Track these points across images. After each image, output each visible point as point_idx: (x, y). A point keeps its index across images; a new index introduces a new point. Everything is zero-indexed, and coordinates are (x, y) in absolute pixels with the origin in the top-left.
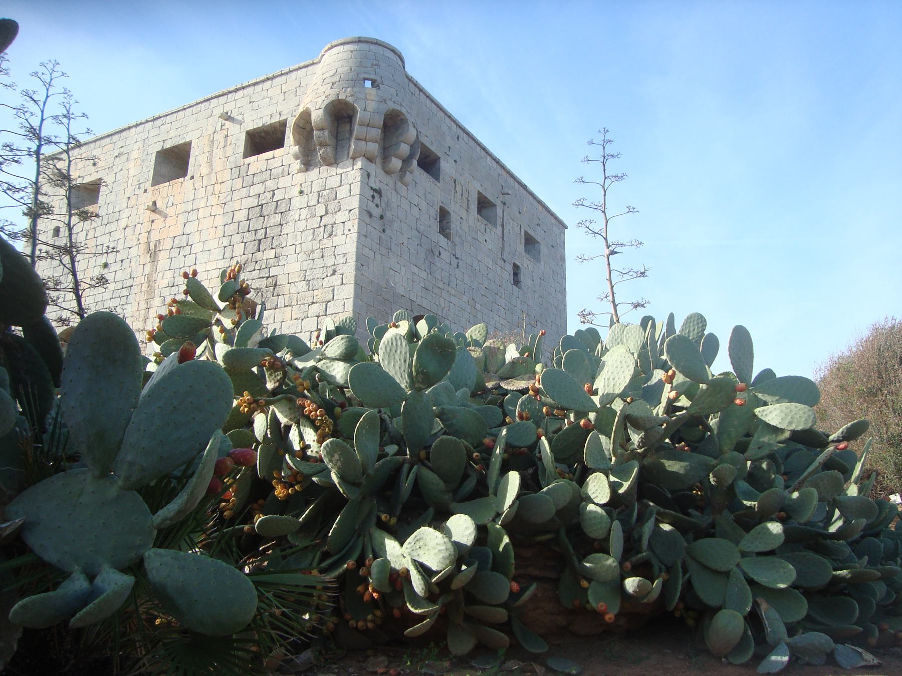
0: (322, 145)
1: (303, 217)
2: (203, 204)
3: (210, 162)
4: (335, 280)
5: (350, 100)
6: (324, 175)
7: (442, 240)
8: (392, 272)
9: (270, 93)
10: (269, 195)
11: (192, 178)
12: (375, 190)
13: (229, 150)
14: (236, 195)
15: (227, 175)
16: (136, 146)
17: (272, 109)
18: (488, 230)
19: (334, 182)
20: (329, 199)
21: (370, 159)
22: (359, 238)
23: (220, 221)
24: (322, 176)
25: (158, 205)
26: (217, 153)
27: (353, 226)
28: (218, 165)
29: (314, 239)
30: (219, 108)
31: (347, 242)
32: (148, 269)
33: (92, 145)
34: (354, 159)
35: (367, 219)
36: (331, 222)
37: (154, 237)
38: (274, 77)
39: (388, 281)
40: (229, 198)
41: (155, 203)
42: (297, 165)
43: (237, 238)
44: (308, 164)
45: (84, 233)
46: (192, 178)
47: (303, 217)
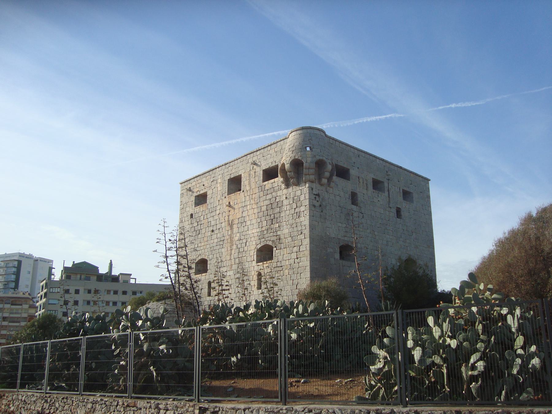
0: (292, 178)
1: (288, 209)
2: (248, 203)
3: (250, 184)
4: (302, 237)
5: (300, 158)
6: (294, 190)
7: (354, 207)
8: (328, 229)
9: (271, 152)
10: (274, 199)
11: (243, 191)
12: (316, 195)
13: (257, 178)
14: (262, 199)
15: (257, 190)
16: (219, 177)
17: (271, 160)
18: (380, 195)
19: (298, 193)
20: (297, 200)
21: (312, 182)
22: (310, 218)
23: (256, 211)
24: (294, 191)
25: (231, 204)
26: (252, 181)
27: (307, 213)
28: (253, 186)
29: (293, 219)
30: (250, 159)
31: (305, 220)
32: (229, 233)
33: (202, 176)
34: (305, 183)
35: (313, 209)
36: (299, 211)
37: (231, 218)
38: (271, 145)
39: (326, 233)
40: (258, 201)
41: (229, 203)
42: (283, 186)
43: (263, 219)
44: (288, 186)
45: (202, 217)
46: (243, 191)
47: (288, 209)
